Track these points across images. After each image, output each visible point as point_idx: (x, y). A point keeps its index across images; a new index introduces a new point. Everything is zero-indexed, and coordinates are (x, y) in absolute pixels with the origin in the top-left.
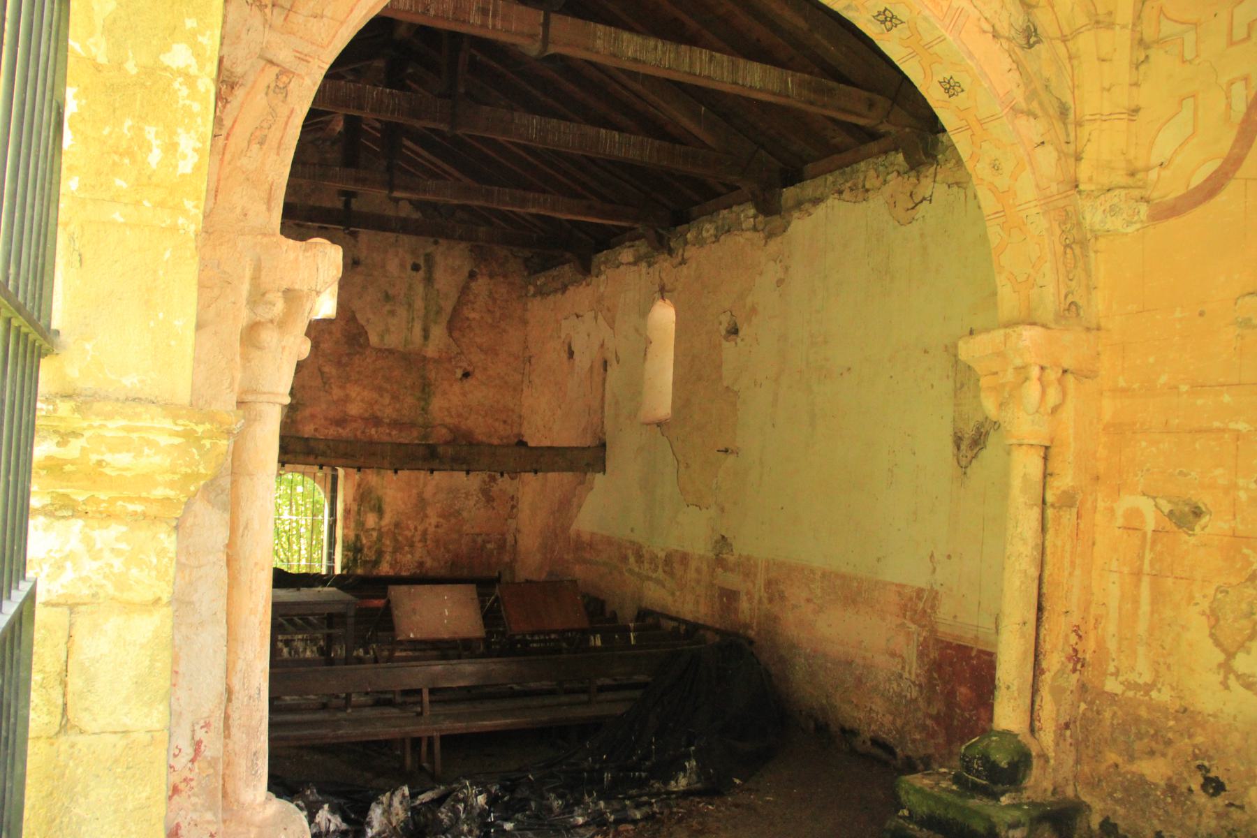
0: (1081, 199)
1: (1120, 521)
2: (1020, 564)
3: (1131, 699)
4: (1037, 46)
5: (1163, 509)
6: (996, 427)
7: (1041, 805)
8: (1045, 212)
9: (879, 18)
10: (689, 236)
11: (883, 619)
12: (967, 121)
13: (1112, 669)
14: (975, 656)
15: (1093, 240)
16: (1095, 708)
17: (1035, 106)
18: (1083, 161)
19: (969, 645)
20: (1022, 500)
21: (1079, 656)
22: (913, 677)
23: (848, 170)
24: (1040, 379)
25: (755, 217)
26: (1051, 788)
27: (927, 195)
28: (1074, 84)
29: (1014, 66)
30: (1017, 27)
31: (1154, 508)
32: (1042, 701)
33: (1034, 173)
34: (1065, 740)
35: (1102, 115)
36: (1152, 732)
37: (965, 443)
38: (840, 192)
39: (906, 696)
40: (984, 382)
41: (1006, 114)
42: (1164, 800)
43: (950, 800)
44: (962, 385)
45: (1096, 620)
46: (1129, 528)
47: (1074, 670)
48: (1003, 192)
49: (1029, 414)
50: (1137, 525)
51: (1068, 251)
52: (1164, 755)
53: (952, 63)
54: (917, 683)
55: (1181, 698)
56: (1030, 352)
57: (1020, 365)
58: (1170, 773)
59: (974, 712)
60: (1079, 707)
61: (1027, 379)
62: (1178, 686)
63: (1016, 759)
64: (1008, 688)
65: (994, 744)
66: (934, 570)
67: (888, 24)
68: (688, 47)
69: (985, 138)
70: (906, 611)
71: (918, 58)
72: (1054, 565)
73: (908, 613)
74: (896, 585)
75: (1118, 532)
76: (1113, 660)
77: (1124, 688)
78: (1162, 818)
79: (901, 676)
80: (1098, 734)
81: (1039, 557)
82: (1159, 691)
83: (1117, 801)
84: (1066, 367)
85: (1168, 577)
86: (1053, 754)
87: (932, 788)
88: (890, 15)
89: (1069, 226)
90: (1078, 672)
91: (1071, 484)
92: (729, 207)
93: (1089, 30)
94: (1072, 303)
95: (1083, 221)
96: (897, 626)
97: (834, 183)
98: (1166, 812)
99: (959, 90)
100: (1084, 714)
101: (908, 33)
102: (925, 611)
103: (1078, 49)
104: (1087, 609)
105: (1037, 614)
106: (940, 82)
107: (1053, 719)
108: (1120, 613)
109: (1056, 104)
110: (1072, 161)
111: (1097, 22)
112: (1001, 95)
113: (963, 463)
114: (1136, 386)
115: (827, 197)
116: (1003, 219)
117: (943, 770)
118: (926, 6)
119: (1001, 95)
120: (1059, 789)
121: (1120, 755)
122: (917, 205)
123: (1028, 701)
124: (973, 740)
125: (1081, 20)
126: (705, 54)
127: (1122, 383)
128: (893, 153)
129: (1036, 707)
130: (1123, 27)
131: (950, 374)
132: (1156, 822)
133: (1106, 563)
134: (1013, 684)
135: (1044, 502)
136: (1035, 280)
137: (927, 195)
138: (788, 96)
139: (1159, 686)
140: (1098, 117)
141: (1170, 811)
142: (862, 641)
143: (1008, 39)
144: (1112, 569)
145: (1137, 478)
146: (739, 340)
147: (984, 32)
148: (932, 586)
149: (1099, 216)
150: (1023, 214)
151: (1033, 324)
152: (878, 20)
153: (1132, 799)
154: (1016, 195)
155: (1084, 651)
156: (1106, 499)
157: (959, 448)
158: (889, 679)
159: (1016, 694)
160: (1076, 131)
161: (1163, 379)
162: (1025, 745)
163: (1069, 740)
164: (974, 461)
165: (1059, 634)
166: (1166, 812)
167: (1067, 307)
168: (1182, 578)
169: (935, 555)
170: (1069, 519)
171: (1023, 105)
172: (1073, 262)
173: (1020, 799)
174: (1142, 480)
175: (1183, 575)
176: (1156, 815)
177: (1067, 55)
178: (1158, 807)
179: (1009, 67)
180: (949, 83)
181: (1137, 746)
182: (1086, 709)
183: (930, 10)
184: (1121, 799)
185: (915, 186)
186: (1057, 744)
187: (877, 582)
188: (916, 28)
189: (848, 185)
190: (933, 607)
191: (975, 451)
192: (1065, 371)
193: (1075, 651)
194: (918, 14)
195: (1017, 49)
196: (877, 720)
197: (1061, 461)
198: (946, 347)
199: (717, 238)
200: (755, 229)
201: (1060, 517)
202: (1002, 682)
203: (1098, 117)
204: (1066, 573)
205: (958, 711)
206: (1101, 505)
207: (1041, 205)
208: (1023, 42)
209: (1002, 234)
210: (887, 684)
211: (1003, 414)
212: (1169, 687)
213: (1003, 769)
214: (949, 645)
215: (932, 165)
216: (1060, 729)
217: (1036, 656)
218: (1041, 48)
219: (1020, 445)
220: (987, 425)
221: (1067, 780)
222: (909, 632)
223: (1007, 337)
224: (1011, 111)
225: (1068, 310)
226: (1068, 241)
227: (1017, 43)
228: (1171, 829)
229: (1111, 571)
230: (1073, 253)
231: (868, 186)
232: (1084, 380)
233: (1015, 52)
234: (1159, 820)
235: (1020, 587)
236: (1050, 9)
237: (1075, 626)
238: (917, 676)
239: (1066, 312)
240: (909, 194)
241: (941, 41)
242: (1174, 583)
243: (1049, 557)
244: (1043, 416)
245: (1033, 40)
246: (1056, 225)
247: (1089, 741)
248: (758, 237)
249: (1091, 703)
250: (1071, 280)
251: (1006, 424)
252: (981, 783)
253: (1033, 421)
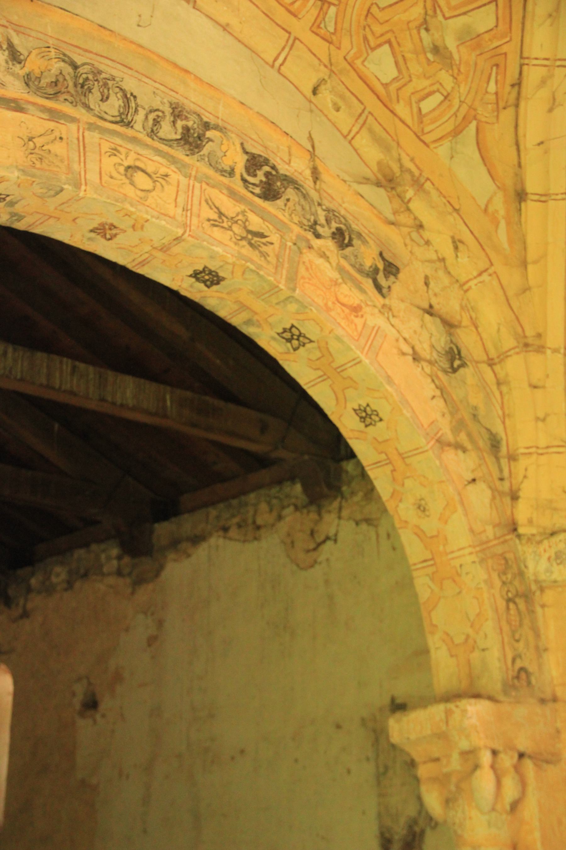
0: (521, 544)
4: (462, 371)
8: (482, 561)
9: (284, 335)
10: (33, 581)
12: (386, 455)
15: (538, 593)
17: (463, 438)
18: (520, 500)
23: (235, 502)
24: (493, 767)
25: (119, 558)
27: (332, 532)
28: (504, 413)
29: (438, 393)
30: (439, 349)
33: (466, 515)
35: (538, 448)
38: (225, 529)
40: (423, 771)
41: (431, 448)
44: (386, 768)
48: (432, 537)
51: (512, 605)
53: (368, 389)
56: (477, 732)
61: (476, 767)
67: (295, 343)
68: (45, 355)
69: (408, 474)
71: (329, 382)
84: (522, 748)
88: (297, 333)
89: (509, 576)
92: (86, 545)
93: (517, 353)
95: (525, 570)
97: (218, 517)
99: (377, 419)
101: (318, 354)
103: (507, 375)
106: (355, 410)
109: (486, 436)
110: (507, 500)
111: (526, 345)
112: (426, 426)
115: (211, 534)
116: (433, 569)
118: (339, 324)
119: (426, 426)
122: (319, 545)
125: (509, 342)
126: (67, 364)
128: (289, 483)
130: (555, 351)
136: (475, 642)
137: (332, 532)
138: (165, 416)
140: (533, 450)
143: (430, 362)
146: (98, 717)
147: (404, 354)
149: (543, 564)
150: (456, 563)
151: (477, 696)
152: (283, 338)
154: (446, 539)
160: (510, 467)
167: (515, 674)
171: (450, 437)
172: (518, 619)
177: (494, 380)
179: (433, 394)
180: (365, 411)
183: (343, 328)
185: (317, 522)
188: (328, 348)
189: (235, 520)
192: (521, 755)
194: (330, 333)
195: (440, 374)
198: (363, 720)
199: (70, 585)
200: (119, 573)
203: (533, 450)
207: (477, 552)
208: (446, 365)
209: (433, 586)
215: (335, 498)
218: (467, 373)
220: (421, 822)
223: (448, 713)
224: (437, 444)
226: (510, 595)
227: (440, 366)
230: (518, 609)
231: (259, 521)
232: (545, 765)
233: (438, 377)
236: (474, 329)
239: (516, 681)
240: (309, 532)
241: (355, 364)
245: (457, 363)
246: (495, 576)
248: (123, 583)
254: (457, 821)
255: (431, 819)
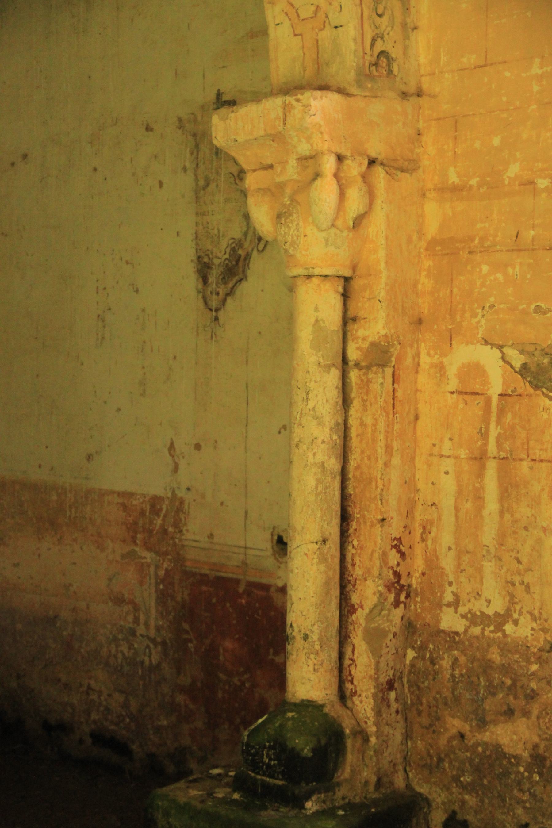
1: (453, 384)
2: (314, 454)
3: (477, 637)
5: (513, 363)
6: (261, 247)
7: (362, 806)
11: (101, 547)
13: (448, 597)
14: (244, 592)
16: (428, 655)
19: (234, 576)
20: (313, 359)
21: (402, 582)
22: (152, 633)
24: (336, 175)
26: (374, 779)
31: (501, 363)
32: (353, 652)
34: (389, 706)
36: (509, 682)
37: (214, 272)
39: (142, 663)
42: (530, 777)
43: (232, 817)
45: (424, 528)
46: (466, 393)
47: (397, 603)
49: (320, 230)
50: (478, 388)
52: (526, 714)
54: (159, 640)
55: (545, 630)
56: (322, 133)
57: (307, 153)
58: (536, 739)
59: (246, 676)
60: (405, 656)
61: (317, 175)
62: (540, 613)
63: (323, 742)
64: (306, 637)
65: (290, 723)
66: (176, 469)
70: (136, 532)
72: (363, 452)
73: (139, 536)
74: (119, 494)
75: (451, 399)
76: (450, 584)
77: (467, 623)
78: (528, 805)
79: (133, 632)
80: (434, 693)
81: (340, 442)
82: (516, 623)
83: (464, 787)
84: (373, 155)
85: (521, 460)
86: (374, 729)
87: (202, 802)
90: (402, 606)
91: (383, 332)
94: (382, 52)
96: (123, 556)
98: (533, 795)
100: (412, 665)
102: (165, 532)
104: (409, 514)
105: (341, 525)
107: (371, 677)
108: (457, 517)
113: (214, 304)
114: (474, 182)
117: (216, 771)
120: (385, 779)
121: (466, 719)
123: (335, 655)
124: (260, 721)
127: (453, 178)
129: (347, 662)
131: (188, 164)
132: (520, 811)
133: (434, 445)
134: (312, 632)
135: (345, 360)
139: (516, 616)
141: (537, 793)
142: (70, 585)
144: (443, 453)
145: (476, 320)
148: (174, 491)
151: (324, 88)
153: (485, 782)
155: (409, 574)
156: (432, 352)
157: (205, 281)
158: (115, 639)
159: (317, 647)
161: (514, 170)
162: (335, 720)
163: (394, 706)
164: (229, 300)
165: (373, 551)
166: (533, 795)
167: (374, 60)
168: (542, 461)
169: (176, 445)
170: (382, 384)
173: (332, 800)
174: (483, 322)
175: (544, 456)
176: (520, 802)
178: (521, 790)
181: (488, 705)
182: (415, 658)
184: (469, 784)
186: (378, 713)
187: (89, 491)
190: (177, 524)
191: (230, 285)
192: (372, 162)
193: (397, 574)
196: (100, 704)
197: (369, 299)
198: (180, 120)
201: (369, 381)
202: (296, 629)
204: (381, 462)
205: (222, 676)
206: (425, 360)
210: (113, 646)
211: (283, 230)
212: (528, 617)
213: (305, 759)
214: (204, 579)
216: (382, 691)
217: (343, 587)
219: (309, 277)
221: (395, 765)
222: (142, 564)
223: (287, 108)
225: (376, 64)
228: (540, 819)
229: (442, 456)
234: (524, 808)
235: (317, 488)
237: (395, 539)
238: (158, 629)
242: (531, 468)
243: (354, 442)
244: (342, 232)
247: (421, 704)
249: (423, 648)
250: (380, 16)
251: (287, 246)
252: (275, 784)
253: (327, 241)
254: (289, 239)
255: (260, 239)
